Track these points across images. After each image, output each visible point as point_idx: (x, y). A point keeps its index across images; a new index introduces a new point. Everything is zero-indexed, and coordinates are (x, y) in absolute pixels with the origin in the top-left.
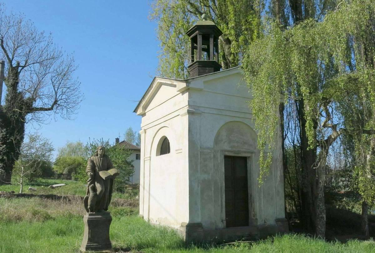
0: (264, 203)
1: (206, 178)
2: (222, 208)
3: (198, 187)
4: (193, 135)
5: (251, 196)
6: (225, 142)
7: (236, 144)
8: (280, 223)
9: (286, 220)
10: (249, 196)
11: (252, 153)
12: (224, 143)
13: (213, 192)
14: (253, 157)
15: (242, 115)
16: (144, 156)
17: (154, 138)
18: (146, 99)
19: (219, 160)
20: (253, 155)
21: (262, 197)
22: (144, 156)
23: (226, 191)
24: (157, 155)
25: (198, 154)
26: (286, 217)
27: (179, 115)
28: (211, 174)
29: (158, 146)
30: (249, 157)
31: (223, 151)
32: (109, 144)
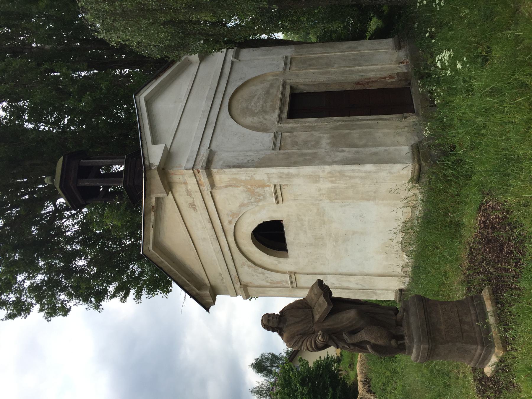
0: (369, 65)
1: (328, 141)
2: (381, 119)
3: (343, 151)
4: (248, 161)
5: (358, 83)
6: (263, 117)
7: (269, 104)
8: (402, 43)
9: (396, 36)
10: (359, 87)
11: (284, 83)
12: (265, 119)
13: (352, 132)
14: (292, 81)
15: (220, 96)
16: (289, 288)
17: (255, 264)
18: (174, 270)
19: (295, 126)
20: (288, 81)
21: (360, 68)
22: (289, 288)
23: (349, 116)
24: (286, 256)
25: (284, 154)
26: (392, 37)
27: (211, 192)
28: (321, 135)
29: (271, 255)
30: (292, 88)
31: (280, 120)
32: (269, 396)
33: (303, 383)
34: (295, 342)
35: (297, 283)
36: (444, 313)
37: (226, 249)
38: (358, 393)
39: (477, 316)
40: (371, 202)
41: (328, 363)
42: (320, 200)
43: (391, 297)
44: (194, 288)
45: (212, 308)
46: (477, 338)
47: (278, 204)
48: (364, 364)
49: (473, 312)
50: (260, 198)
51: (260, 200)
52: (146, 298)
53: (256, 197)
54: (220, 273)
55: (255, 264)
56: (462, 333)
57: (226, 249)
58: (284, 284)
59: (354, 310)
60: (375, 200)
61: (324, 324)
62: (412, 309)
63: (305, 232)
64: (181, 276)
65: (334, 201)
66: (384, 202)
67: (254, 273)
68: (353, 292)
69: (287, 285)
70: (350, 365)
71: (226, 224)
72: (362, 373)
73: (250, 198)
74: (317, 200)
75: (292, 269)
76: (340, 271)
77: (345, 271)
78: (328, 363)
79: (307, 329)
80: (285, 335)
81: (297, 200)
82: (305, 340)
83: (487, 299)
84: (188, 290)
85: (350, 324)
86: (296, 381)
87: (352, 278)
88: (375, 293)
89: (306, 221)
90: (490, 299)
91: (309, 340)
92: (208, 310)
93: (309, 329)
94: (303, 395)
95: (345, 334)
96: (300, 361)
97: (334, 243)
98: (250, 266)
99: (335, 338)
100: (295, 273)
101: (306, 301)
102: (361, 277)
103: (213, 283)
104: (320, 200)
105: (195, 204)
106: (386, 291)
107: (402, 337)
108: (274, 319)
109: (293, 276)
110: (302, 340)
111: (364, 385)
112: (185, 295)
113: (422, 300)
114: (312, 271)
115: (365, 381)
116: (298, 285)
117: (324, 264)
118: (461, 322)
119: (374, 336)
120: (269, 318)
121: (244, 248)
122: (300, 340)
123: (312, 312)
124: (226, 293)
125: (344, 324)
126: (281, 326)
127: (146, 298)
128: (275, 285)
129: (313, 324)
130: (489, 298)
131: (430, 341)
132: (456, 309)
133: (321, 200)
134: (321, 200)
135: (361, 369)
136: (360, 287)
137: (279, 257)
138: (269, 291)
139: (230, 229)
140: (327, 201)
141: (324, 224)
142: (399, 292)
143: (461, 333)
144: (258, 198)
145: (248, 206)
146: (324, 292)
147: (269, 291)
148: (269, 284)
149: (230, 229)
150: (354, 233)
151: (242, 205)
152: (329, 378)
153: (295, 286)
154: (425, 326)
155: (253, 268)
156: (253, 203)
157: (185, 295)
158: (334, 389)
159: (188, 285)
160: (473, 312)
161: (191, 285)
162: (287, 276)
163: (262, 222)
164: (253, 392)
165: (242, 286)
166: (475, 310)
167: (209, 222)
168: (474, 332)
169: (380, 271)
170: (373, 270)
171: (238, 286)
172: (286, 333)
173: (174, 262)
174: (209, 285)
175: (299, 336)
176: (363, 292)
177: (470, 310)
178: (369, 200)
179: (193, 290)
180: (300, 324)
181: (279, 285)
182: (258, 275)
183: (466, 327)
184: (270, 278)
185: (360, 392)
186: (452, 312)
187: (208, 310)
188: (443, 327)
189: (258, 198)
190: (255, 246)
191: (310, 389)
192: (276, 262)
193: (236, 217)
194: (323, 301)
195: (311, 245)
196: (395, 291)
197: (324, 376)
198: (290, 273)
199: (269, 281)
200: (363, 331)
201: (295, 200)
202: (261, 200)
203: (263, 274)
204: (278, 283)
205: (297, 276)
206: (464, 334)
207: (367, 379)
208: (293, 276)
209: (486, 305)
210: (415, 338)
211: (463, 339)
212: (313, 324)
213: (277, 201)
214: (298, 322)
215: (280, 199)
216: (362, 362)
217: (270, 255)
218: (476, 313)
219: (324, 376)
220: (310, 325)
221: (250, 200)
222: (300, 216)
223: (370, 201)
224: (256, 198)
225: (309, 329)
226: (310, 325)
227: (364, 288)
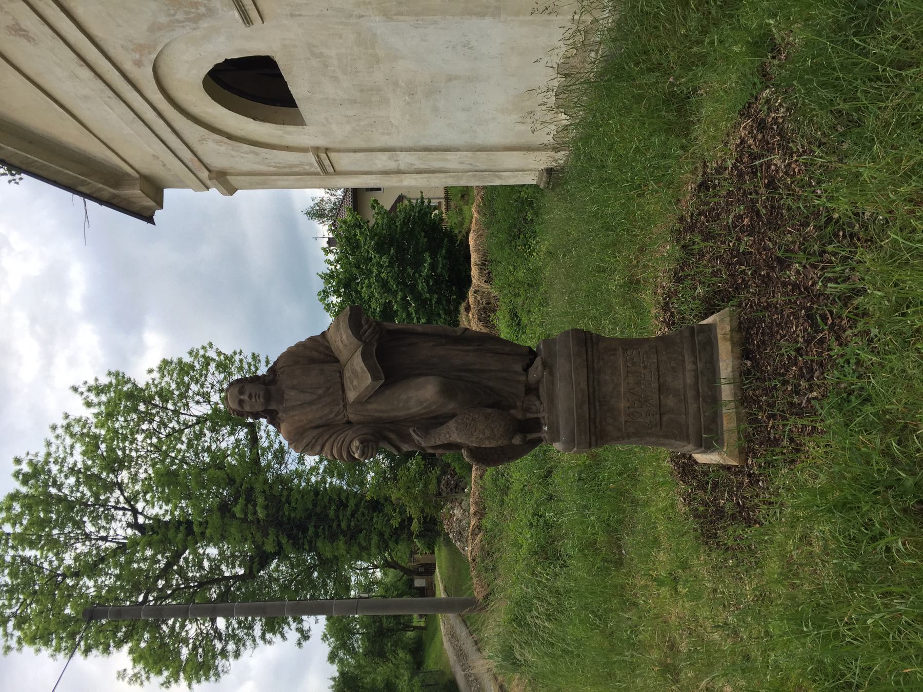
17: (230, 137)
22: (318, 174)
33: (380, 248)
34: (307, 445)
35: (334, 165)
36: (628, 372)
37: (150, 115)
38: (471, 282)
39: (696, 377)
40: (488, 21)
41: (422, 212)
42: (361, 16)
43: (530, 179)
44: (101, 186)
45: (158, 215)
46: (690, 427)
47: (252, 26)
48: (481, 235)
49: (689, 366)
50: (199, 11)
51: (199, 18)
52: (10, 182)
53: (187, 9)
54: (154, 156)
55: (230, 137)
56: (660, 414)
57: (150, 115)
58: (307, 167)
59: (431, 379)
60: (500, 15)
61: (370, 407)
62: (562, 366)
63: (335, 79)
64: (60, 169)
65: (394, 17)
66: (521, 18)
67: (234, 153)
68: (453, 177)
69: (313, 170)
70: (463, 196)
71: (128, 66)
72: (477, 251)
73: (172, 12)
74: (351, 16)
75: (321, 142)
76: (424, 143)
77: (434, 142)
78: (422, 212)
79: (330, 416)
80: (283, 426)
81: (300, 15)
82: (327, 441)
83: (725, 339)
84: (88, 192)
85: (424, 411)
86: (368, 246)
87: (450, 156)
88: (500, 177)
89: (332, 57)
90: (731, 339)
91: (335, 444)
92: (150, 219)
93: (336, 415)
94: (382, 266)
95: (414, 431)
96: (373, 207)
97: (407, 98)
98: (221, 142)
99: (392, 436)
100: (327, 150)
101: (327, 344)
102: (470, 154)
103: (145, 170)
104: (361, 16)
105: (23, 27)
106: (521, 173)
107: (535, 425)
108: (253, 400)
109: (323, 156)
110: (321, 441)
111: (481, 270)
112: (85, 202)
113: (586, 343)
114: (363, 145)
115: (484, 264)
116: (337, 168)
117: (389, 134)
118: (660, 389)
119: (477, 438)
120: (242, 397)
121: (195, 110)
122: (316, 441)
123: (341, 373)
124: (182, 185)
125: (412, 411)
126: (273, 406)
127: (10, 182)
128: (287, 170)
129: (345, 406)
130: (728, 336)
131: (593, 439)
132: (655, 361)
133: (363, 16)
134: (363, 16)
135: (476, 245)
136: (469, 167)
137: (284, 124)
138: (277, 180)
139: (145, 77)
140: (378, 19)
141: (378, 62)
142: (545, 174)
143: (658, 417)
144: (193, 10)
145: (174, 30)
146: (365, 343)
147: (277, 180)
148: (272, 169)
149: (145, 77)
150: (450, 79)
151: (155, 28)
152: (425, 237)
153: (331, 170)
154: (586, 407)
155: (227, 144)
156: (183, 22)
157: (85, 202)
158: (433, 256)
159: (83, 183)
160: (689, 366)
161: (91, 181)
162: (311, 158)
163: (221, 60)
164: (308, 213)
165: (214, 175)
166: (695, 363)
167: (81, 66)
168: (686, 413)
169: (510, 140)
170: (494, 139)
171: (204, 174)
172: (285, 424)
173: (30, 142)
174: (136, 175)
175: (316, 432)
176: (474, 176)
177: (684, 361)
178: (482, 15)
179: (101, 190)
180: (314, 407)
181: (297, 170)
182: (245, 155)
183: (670, 402)
184: (272, 159)
185: (474, 281)
186: (645, 367)
187: (150, 219)
188: (623, 405)
189: (193, 10)
190: (220, 106)
191: (392, 258)
192: (280, 133)
193: (150, 53)
194: (362, 368)
195: (355, 102)
196: (537, 173)
197: (417, 233)
198: (316, 150)
199: (274, 165)
200: (452, 424)
201: (292, 15)
202: (204, 15)
203: (256, 154)
204: (291, 166)
205: (333, 155)
206: (665, 418)
207: (485, 261)
208: (323, 156)
209: (720, 351)
210: (562, 432)
211: (661, 428)
212: (345, 406)
213: (247, 20)
214: (311, 403)
215: (253, 14)
216: (478, 232)
217: (261, 120)
218: (696, 370)
219: (417, 233)
220: (337, 409)
221: (174, 15)
222: (314, 46)
223: (486, 18)
224: (187, 13)
225: (336, 415)
226: (337, 409)
227: (476, 168)
